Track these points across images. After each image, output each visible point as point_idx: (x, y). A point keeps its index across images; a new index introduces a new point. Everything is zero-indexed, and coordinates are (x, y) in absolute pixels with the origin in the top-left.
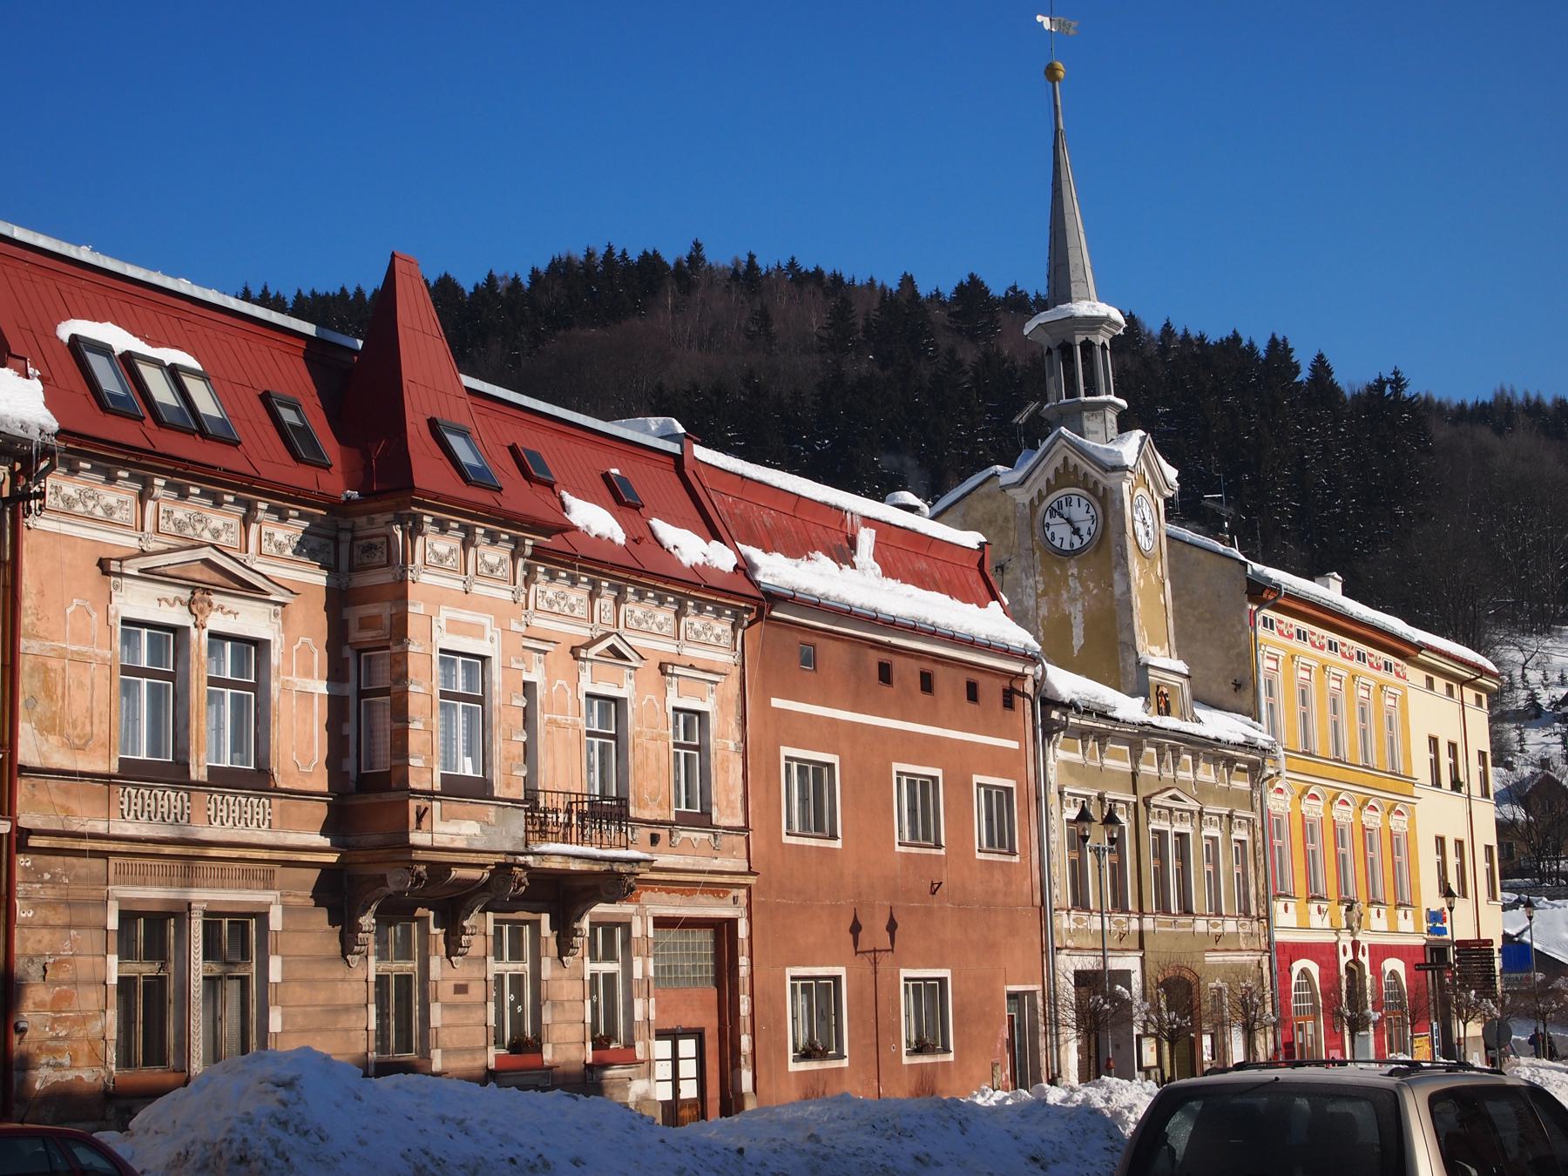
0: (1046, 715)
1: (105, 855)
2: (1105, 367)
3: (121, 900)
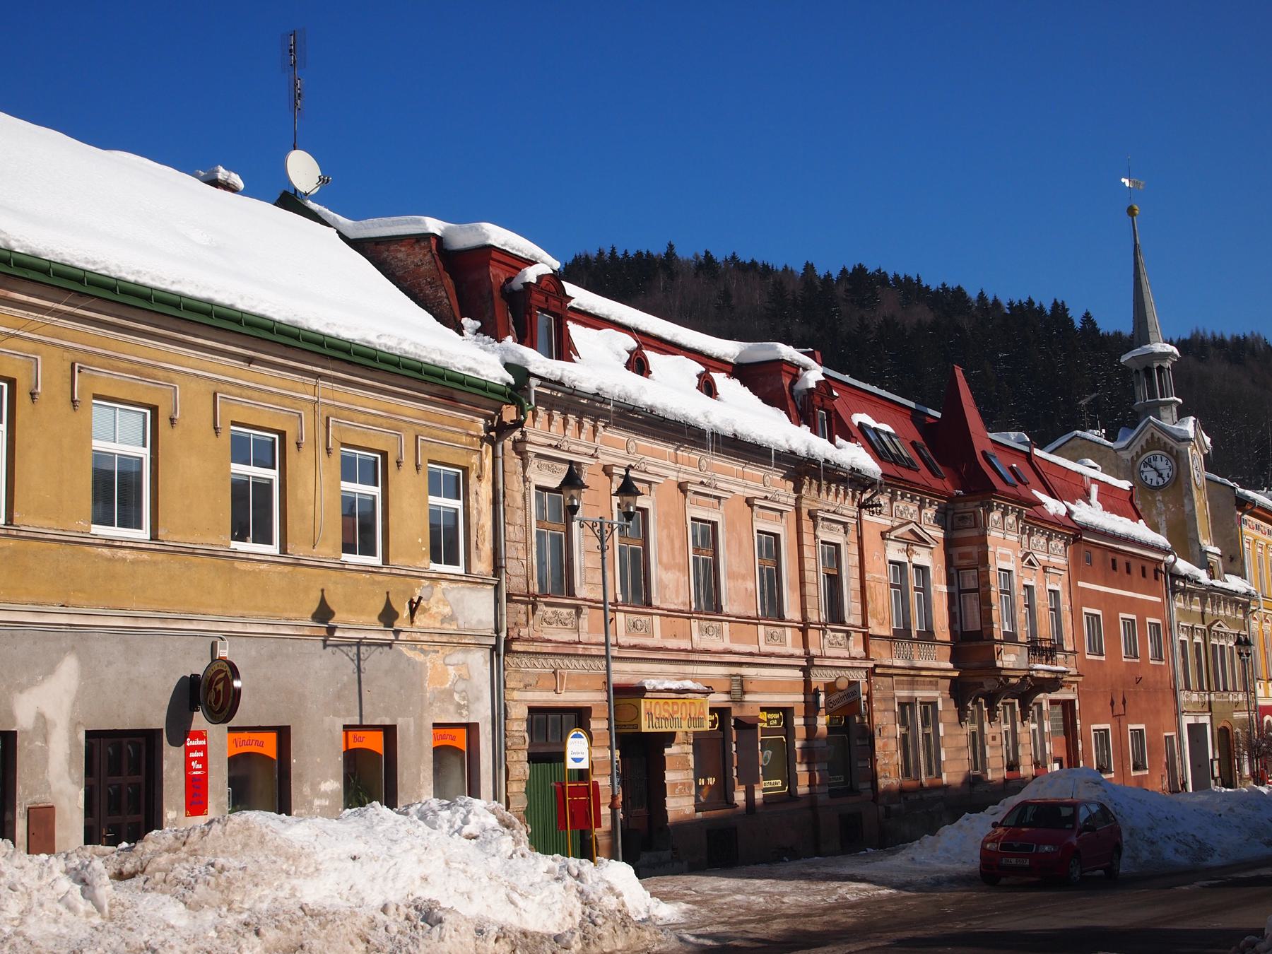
0: (1172, 583)
1: (891, 675)
2: (1169, 379)
3: (898, 697)
